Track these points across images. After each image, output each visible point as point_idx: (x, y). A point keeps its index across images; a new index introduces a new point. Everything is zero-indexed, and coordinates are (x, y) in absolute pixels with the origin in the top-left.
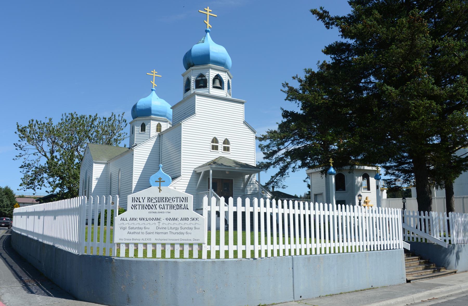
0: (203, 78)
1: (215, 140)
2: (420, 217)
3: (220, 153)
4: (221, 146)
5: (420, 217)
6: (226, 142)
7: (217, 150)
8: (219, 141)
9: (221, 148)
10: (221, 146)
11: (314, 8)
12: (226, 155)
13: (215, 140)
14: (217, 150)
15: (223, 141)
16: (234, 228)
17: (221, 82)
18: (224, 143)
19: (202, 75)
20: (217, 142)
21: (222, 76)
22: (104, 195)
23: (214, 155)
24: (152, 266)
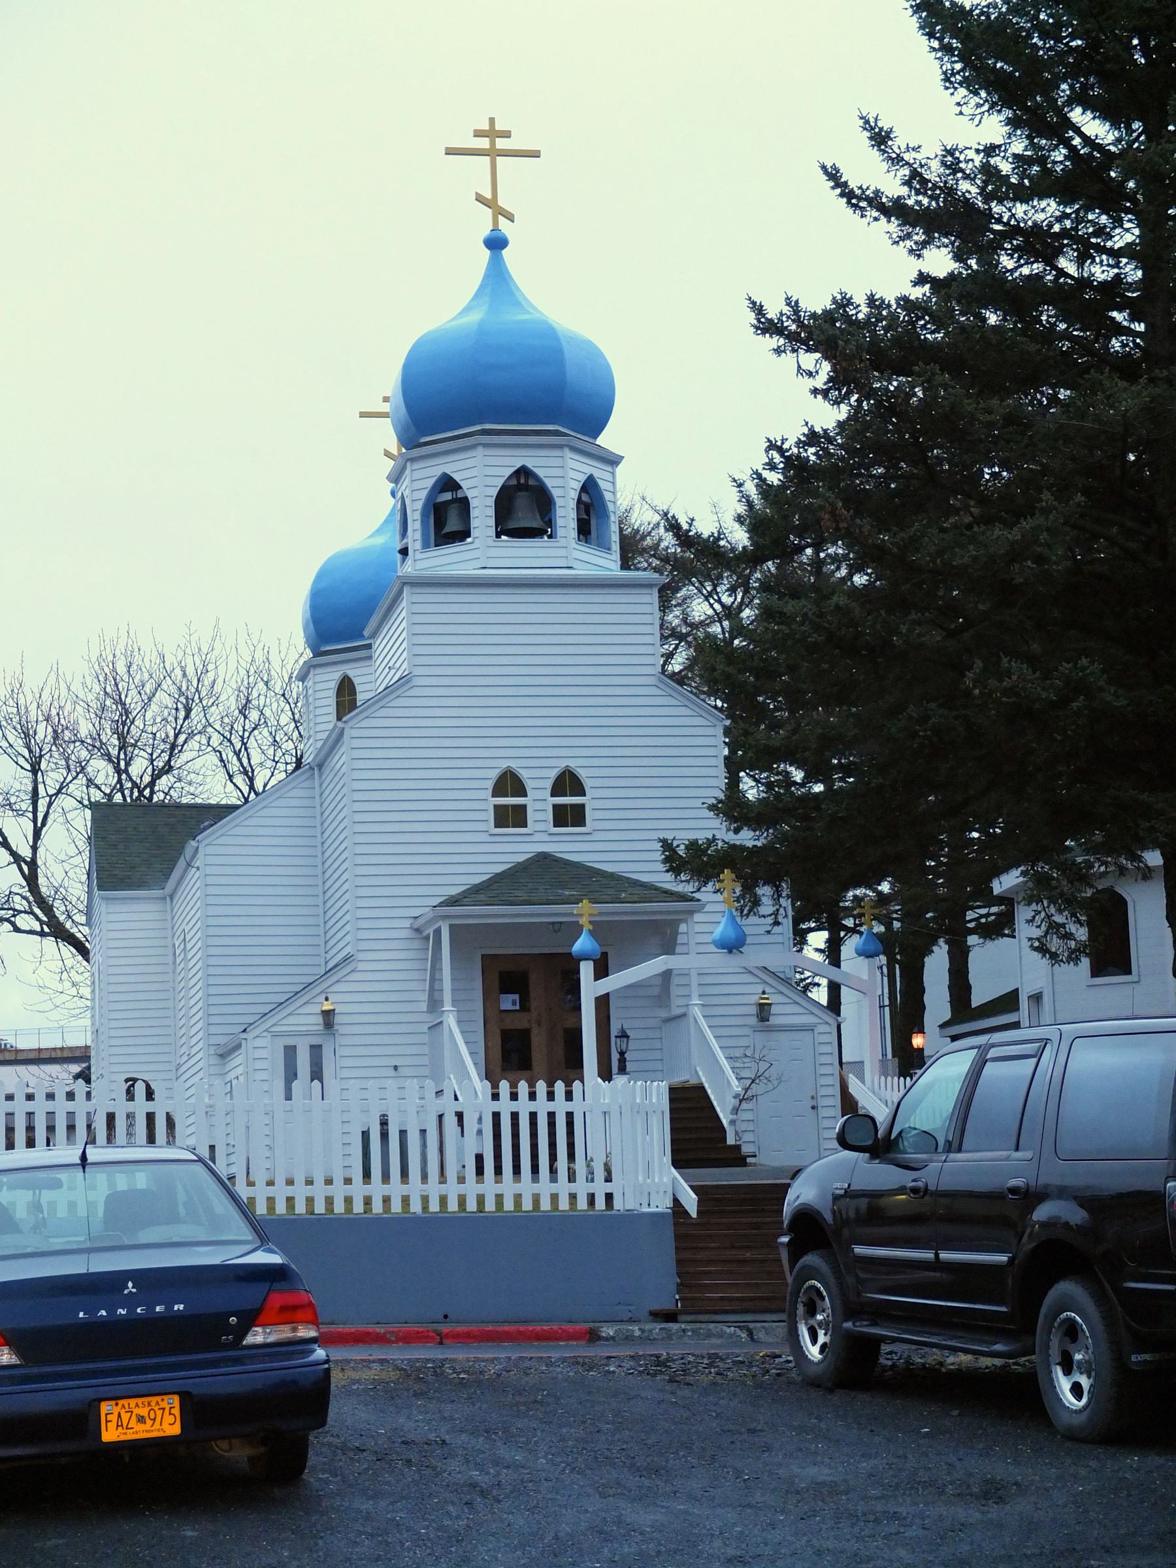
0: (460, 494)
1: (509, 783)
2: (495, 1106)
3: (540, 836)
4: (539, 802)
5: (495, 1106)
6: (568, 783)
7: (524, 824)
8: (529, 785)
9: (540, 816)
10: (539, 802)
11: (776, 437)
12: (569, 846)
13: (509, 783)
14: (524, 824)
15: (549, 784)
16: (514, 1166)
17: (543, 500)
18: (557, 790)
19: (448, 483)
20: (520, 789)
21: (540, 472)
22: (1011, 1261)
23: (516, 848)
24: (512, 294)
